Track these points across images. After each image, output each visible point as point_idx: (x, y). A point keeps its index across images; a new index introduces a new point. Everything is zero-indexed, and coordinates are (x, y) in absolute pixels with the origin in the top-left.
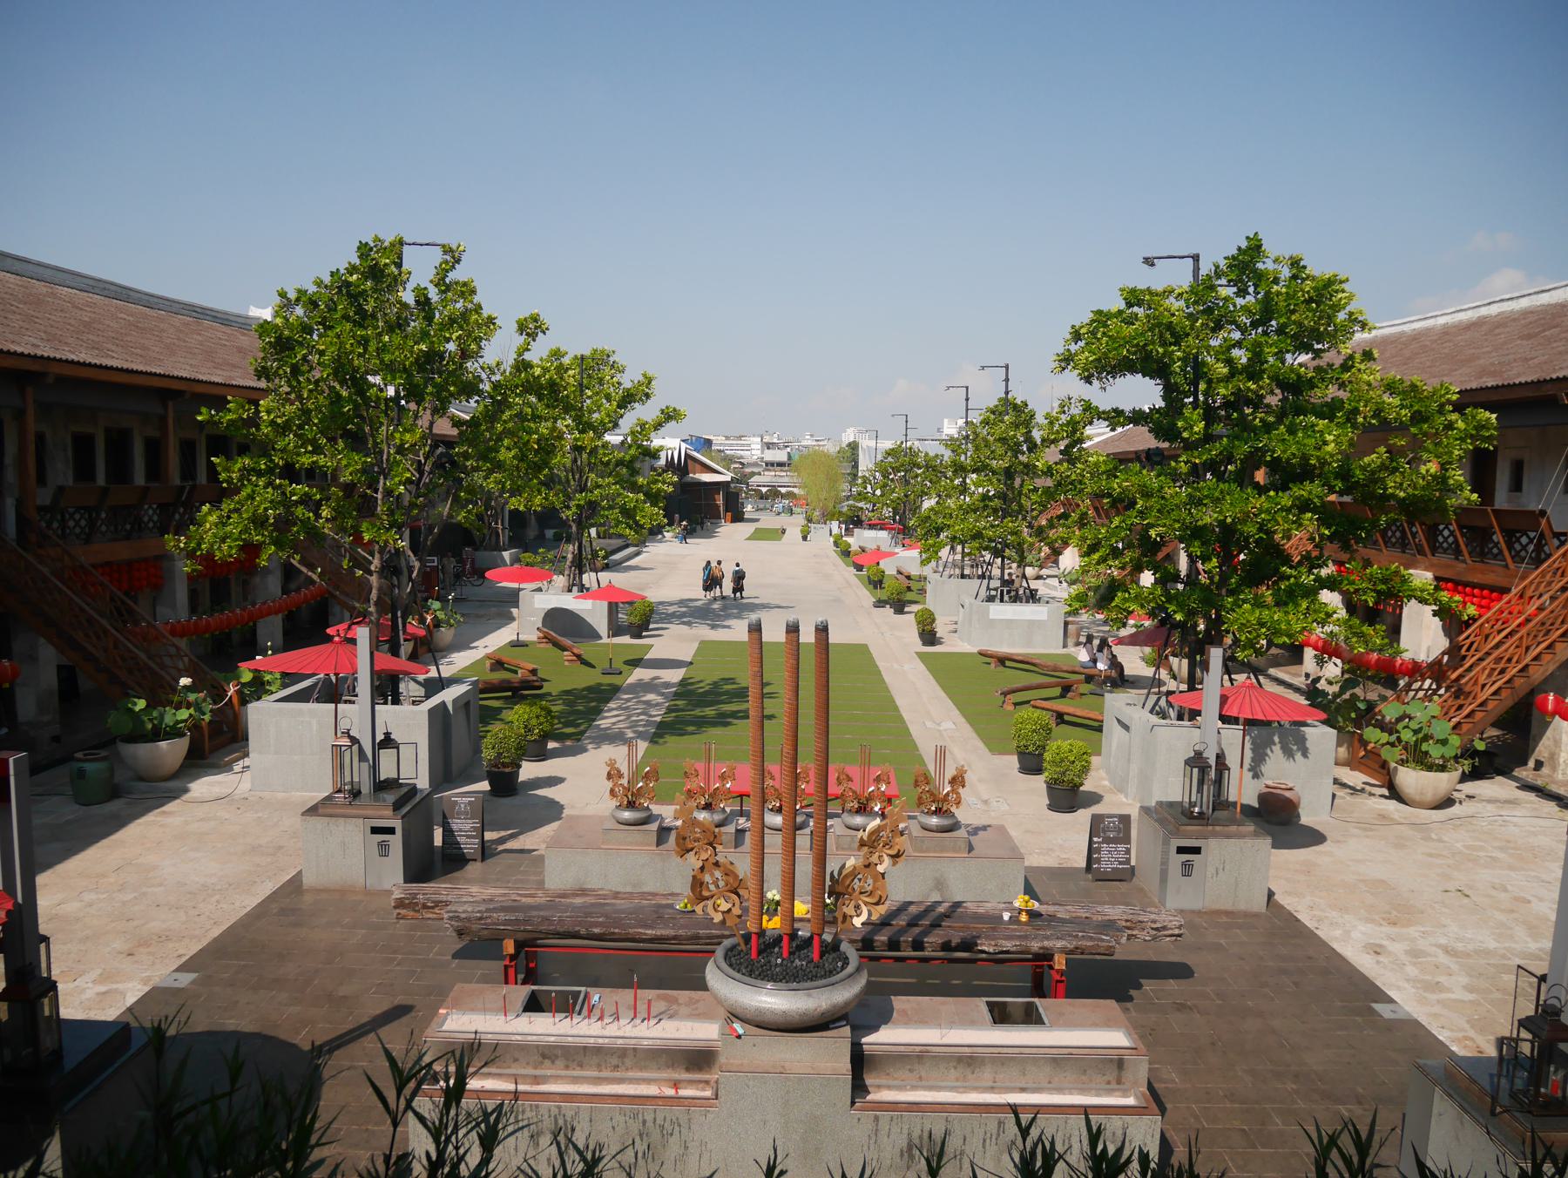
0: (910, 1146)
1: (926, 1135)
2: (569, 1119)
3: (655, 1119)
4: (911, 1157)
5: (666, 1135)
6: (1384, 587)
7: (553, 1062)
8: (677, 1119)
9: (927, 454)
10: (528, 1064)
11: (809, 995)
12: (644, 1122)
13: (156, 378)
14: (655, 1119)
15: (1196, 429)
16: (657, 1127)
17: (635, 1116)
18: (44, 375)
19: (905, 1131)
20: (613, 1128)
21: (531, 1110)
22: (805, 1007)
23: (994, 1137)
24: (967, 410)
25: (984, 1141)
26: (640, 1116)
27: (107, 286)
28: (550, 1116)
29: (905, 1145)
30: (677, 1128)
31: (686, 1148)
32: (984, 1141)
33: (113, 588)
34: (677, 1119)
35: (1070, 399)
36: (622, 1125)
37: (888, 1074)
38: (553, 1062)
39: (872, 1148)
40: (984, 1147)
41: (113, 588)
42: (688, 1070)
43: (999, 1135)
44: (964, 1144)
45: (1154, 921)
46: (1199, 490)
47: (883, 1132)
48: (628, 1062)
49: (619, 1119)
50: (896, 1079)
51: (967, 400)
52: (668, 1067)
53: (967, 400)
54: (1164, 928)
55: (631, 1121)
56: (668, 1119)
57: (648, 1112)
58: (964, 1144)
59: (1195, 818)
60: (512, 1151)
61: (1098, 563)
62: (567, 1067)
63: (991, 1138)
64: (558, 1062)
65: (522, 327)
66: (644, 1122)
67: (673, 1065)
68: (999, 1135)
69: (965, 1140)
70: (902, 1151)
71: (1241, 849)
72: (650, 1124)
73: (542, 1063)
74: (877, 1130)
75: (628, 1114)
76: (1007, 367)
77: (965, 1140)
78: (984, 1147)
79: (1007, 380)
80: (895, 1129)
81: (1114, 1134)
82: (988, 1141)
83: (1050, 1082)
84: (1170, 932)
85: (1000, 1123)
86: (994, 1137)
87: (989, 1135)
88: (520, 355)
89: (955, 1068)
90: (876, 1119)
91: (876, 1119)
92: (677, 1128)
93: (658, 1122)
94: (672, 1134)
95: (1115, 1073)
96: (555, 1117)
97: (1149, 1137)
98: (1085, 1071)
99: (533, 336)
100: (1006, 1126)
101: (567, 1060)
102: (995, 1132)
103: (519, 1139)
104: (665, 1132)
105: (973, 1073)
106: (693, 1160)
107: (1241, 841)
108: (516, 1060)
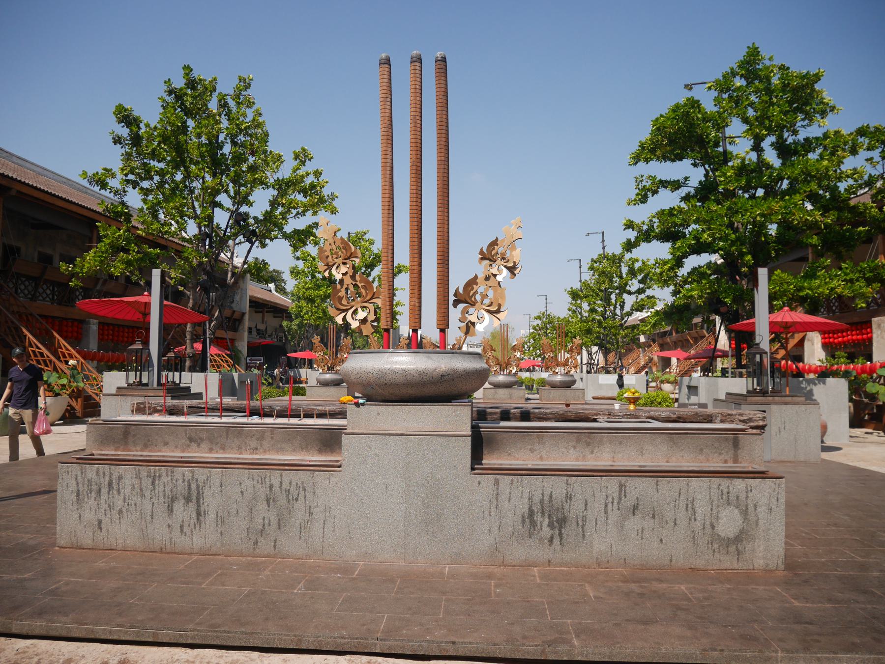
0: (531, 513)
1: (546, 498)
2: (201, 484)
3: (281, 483)
4: (533, 523)
5: (292, 500)
6: (871, 274)
7: (199, 445)
8: (302, 483)
9: (559, 318)
10: (176, 447)
11: (429, 358)
12: (271, 487)
13: (85, 210)
14: (281, 483)
15: (729, 174)
16: (284, 492)
17: (262, 481)
18: (10, 189)
19: (526, 495)
20: (242, 492)
21: (167, 476)
22: (423, 366)
23: (616, 502)
24: (581, 273)
25: (606, 505)
26: (267, 480)
27: (74, 184)
28: (184, 482)
29: (526, 510)
30: (302, 493)
31: (311, 514)
32: (606, 505)
33: (48, 326)
34: (302, 483)
35: (642, 176)
36: (250, 490)
37: (510, 454)
38: (199, 445)
39: (493, 513)
40: (606, 513)
41: (48, 326)
42: (320, 451)
43: (620, 499)
44: (586, 509)
45: (741, 415)
46: (736, 204)
47: (504, 497)
48: (266, 444)
49: (247, 483)
50: (518, 459)
51: (580, 267)
52: (302, 449)
53: (580, 267)
54: (750, 420)
55: (259, 486)
56: (294, 483)
57: (275, 477)
58: (586, 509)
59: (758, 393)
60: (149, 518)
61: (669, 270)
62: (211, 450)
63: (612, 503)
64: (203, 445)
65: (296, 157)
66: (271, 487)
67: (307, 447)
68: (620, 499)
69: (586, 505)
70: (523, 517)
71: (797, 412)
72: (276, 489)
73: (189, 446)
74: (498, 494)
75: (256, 477)
76: (603, 233)
77: (586, 505)
78: (606, 513)
79: (603, 241)
80: (516, 493)
81: (738, 497)
82: (610, 505)
83: (667, 462)
84: (755, 424)
85: (621, 486)
86: (616, 502)
87: (610, 499)
88: (294, 171)
89: (575, 447)
90: (497, 482)
91: (497, 482)
92: (302, 493)
93: (284, 486)
94: (297, 500)
95: (731, 452)
96: (189, 482)
97: (774, 500)
98: (701, 450)
99: (303, 163)
100: (628, 488)
101: (212, 443)
102: (616, 495)
103: (156, 505)
104: (290, 498)
105: (592, 453)
106: (317, 526)
107: (797, 406)
108: (166, 444)
